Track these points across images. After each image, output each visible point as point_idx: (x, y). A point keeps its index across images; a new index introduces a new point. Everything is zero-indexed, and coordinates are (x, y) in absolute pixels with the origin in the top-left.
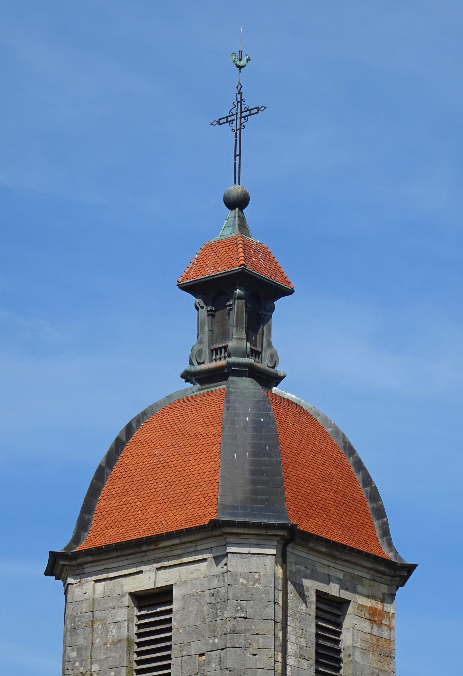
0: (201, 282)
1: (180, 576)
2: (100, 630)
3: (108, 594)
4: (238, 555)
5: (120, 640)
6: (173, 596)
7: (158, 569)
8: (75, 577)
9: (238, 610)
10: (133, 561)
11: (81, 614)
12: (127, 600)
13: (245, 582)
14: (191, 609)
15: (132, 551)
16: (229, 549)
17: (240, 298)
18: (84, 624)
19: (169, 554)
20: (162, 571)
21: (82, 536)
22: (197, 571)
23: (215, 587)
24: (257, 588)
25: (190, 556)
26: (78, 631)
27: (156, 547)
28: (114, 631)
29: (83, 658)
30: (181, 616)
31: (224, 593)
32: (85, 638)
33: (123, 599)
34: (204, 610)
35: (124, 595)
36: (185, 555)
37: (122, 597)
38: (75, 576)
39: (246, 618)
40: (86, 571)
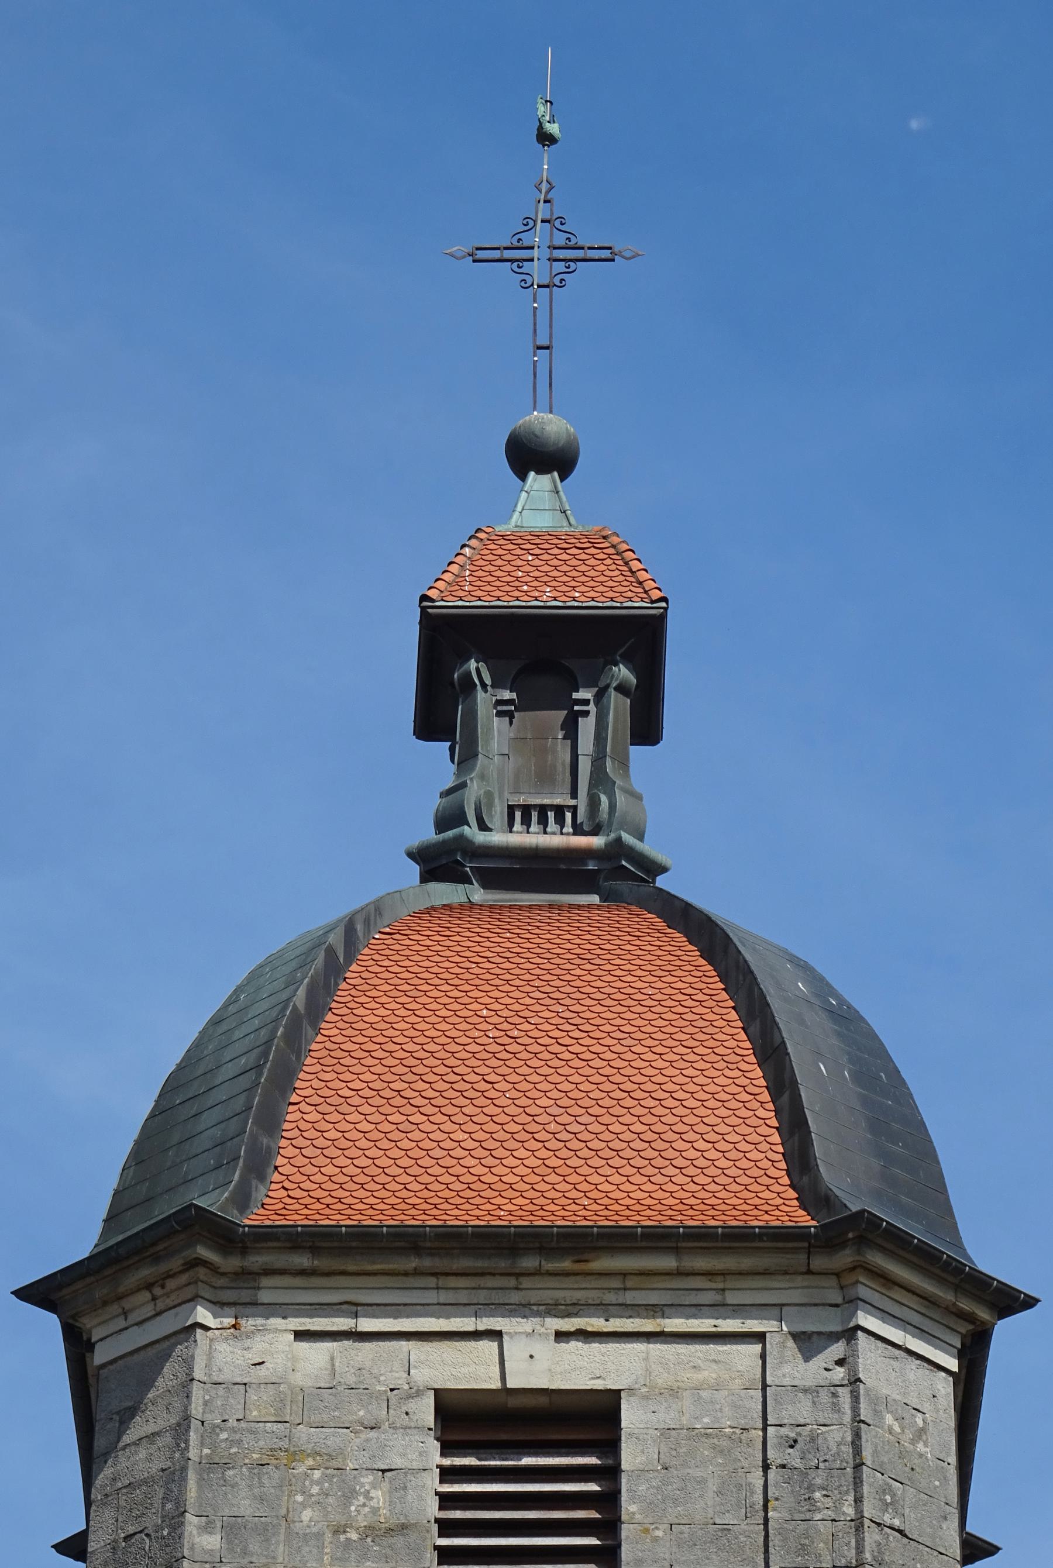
0: (513, 616)
1: (648, 1372)
2: (318, 1483)
3: (351, 1380)
5: (404, 1527)
6: (623, 1424)
7: (561, 1336)
8: (217, 1309)
9: (887, 1504)
10: (463, 1297)
11: (243, 1424)
12: (426, 1411)
13: (897, 1428)
14: (698, 1473)
15: (480, 1264)
16: (867, 1320)
17: (622, 689)
18: (255, 1456)
19: (610, 1298)
20: (575, 1345)
21: (254, 1193)
22: (714, 1366)
23: (802, 1421)
24: (921, 1455)
25: (694, 1316)
26: (231, 1473)
27: (578, 1267)
29: (254, 1560)
30: (658, 1488)
31: (839, 1444)
33: (411, 1406)
35: (419, 1393)
36: (673, 1310)
38: (218, 1305)
39: (900, 1532)
40: (265, 1296)
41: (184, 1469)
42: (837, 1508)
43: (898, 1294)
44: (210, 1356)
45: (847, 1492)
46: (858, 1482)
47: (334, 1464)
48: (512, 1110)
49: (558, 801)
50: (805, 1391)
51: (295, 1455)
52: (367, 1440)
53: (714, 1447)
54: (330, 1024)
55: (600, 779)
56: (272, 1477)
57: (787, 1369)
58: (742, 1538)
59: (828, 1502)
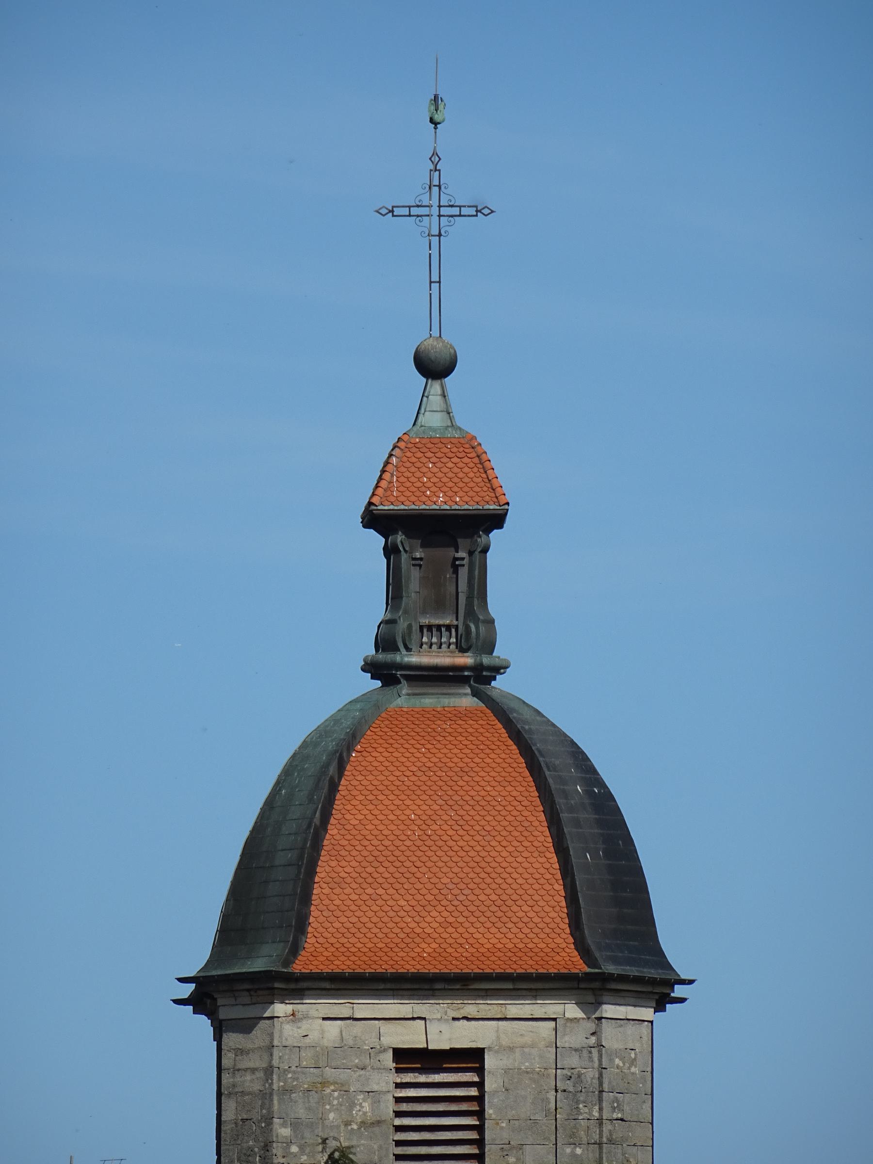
1: (498, 1037)
3: (351, 1043)
4: (613, 1021)
9: (614, 1108)
12: (388, 1059)
13: (621, 1064)
14: (523, 1093)
18: (306, 1086)
23: (574, 1066)
24: (633, 1073)
26: (294, 1095)
28: (365, 1104)
30: (503, 1101)
32: (309, 1109)
33: (382, 1057)
34: (547, 1098)
35: (385, 1050)
37: (380, 1052)
39: (622, 1120)
41: (271, 1094)
42: (590, 1113)
43: (623, 994)
44: (281, 1031)
45: (595, 1105)
46: (600, 1100)
47: (344, 1089)
48: (429, 886)
49: (448, 622)
50: (576, 1050)
51: (325, 1084)
52: (360, 1076)
53: (530, 1079)
54: (332, 830)
55: (470, 613)
56: (314, 1097)
57: (567, 1038)
58: (544, 1127)
59: (586, 1110)
